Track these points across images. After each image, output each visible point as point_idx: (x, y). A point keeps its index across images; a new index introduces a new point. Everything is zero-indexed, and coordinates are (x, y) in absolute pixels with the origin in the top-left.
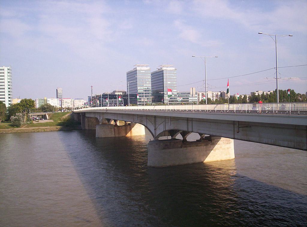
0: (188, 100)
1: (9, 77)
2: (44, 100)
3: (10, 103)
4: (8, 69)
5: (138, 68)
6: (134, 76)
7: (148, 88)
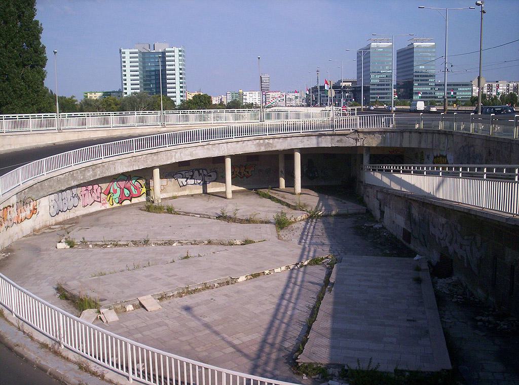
0: (427, 82)
1: (181, 63)
2: (239, 93)
3: (182, 98)
4: (180, 51)
5: (373, 45)
6: (426, 78)
7: (387, 76)
